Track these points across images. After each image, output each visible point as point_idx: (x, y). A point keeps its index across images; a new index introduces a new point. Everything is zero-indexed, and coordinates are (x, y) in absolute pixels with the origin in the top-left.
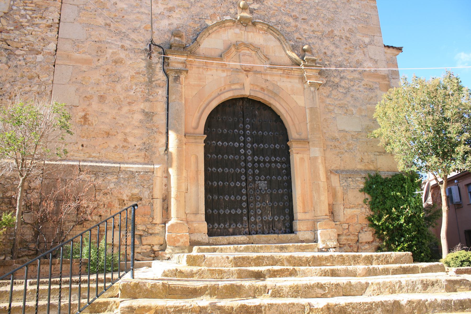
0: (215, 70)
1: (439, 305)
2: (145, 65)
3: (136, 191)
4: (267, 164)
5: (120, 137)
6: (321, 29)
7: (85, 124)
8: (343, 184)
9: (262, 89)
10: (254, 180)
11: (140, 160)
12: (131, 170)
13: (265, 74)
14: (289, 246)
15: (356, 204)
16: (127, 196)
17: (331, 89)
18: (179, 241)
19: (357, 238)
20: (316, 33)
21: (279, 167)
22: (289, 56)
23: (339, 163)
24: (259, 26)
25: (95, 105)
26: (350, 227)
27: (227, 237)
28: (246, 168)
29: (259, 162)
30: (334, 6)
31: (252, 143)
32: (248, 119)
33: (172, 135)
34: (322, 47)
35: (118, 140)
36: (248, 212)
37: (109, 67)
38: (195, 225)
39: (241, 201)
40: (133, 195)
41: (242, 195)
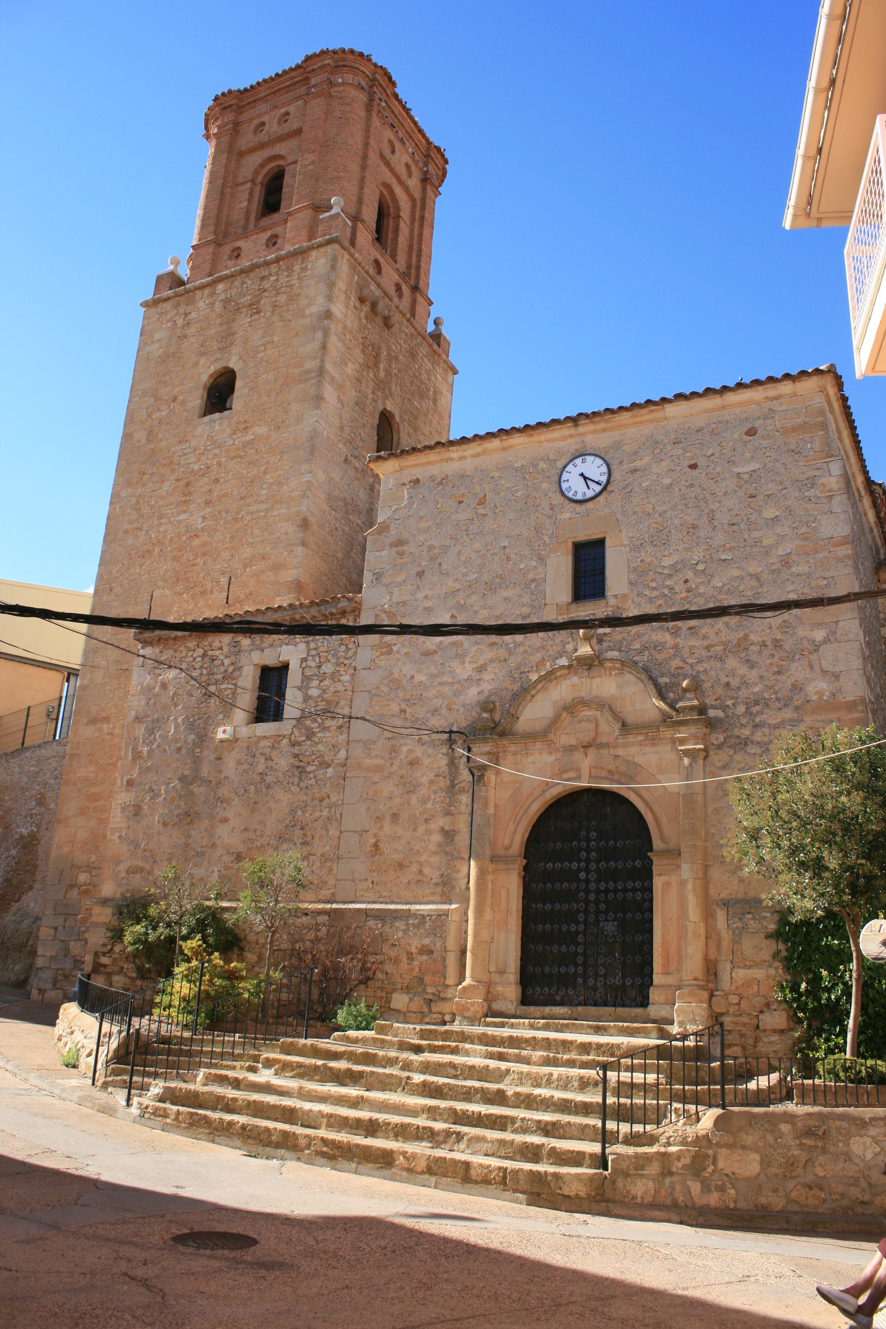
0: (538, 755)
1: (554, 1104)
2: (446, 762)
3: (426, 941)
4: (620, 893)
5: (415, 868)
6: (724, 639)
7: (376, 854)
8: (734, 926)
9: (610, 771)
10: (597, 921)
11: (436, 898)
12: (422, 913)
13: (614, 747)
14: (609, 1026)
15: (758, 960)
16: (417, 948)
17: (732, 752)
18: (469, 1010)
19: (755, 1021)
20: (712, 649)
21: (639, 898)
22: (657, 707)
23: (736, 888)
24: (608, 664)
25: (388, 828)
26: (742, 1001)
27: (541, 1008)
28: (587, 902)
29: (607, 891)
30: (754, 583)
31: (598, 861)
32: (593, 823)
33: (472, 863)
34: (721, 673)
35: (409, 874)
36: (585, 971)
37: (403, 772)
38: (500, 988)
39: (576, 954)
40: (423, 946)
41: (577, 944)
